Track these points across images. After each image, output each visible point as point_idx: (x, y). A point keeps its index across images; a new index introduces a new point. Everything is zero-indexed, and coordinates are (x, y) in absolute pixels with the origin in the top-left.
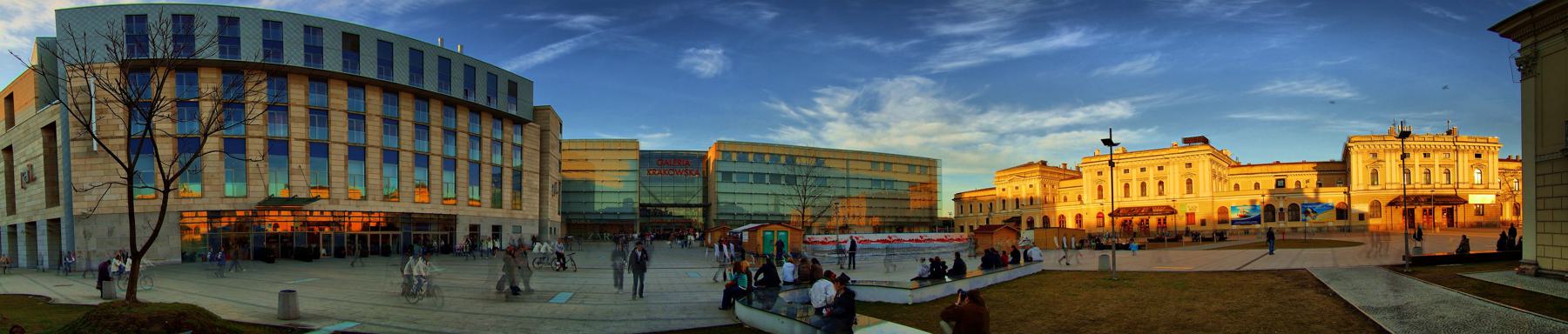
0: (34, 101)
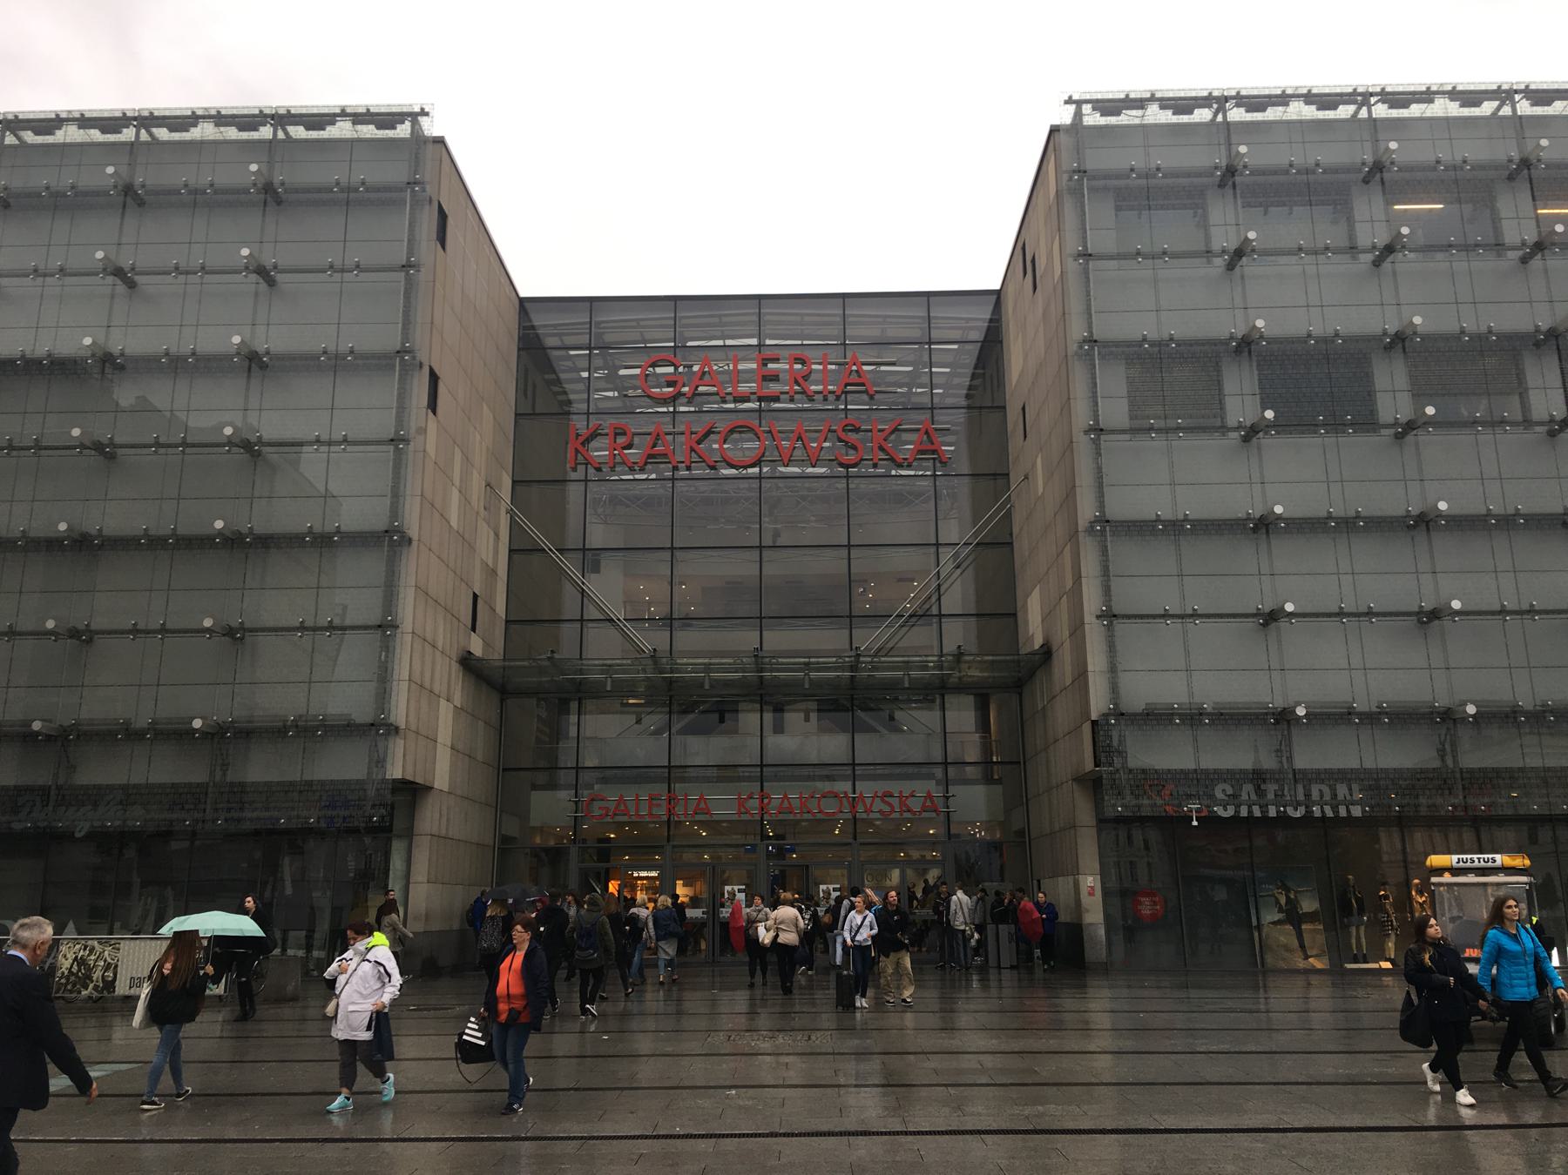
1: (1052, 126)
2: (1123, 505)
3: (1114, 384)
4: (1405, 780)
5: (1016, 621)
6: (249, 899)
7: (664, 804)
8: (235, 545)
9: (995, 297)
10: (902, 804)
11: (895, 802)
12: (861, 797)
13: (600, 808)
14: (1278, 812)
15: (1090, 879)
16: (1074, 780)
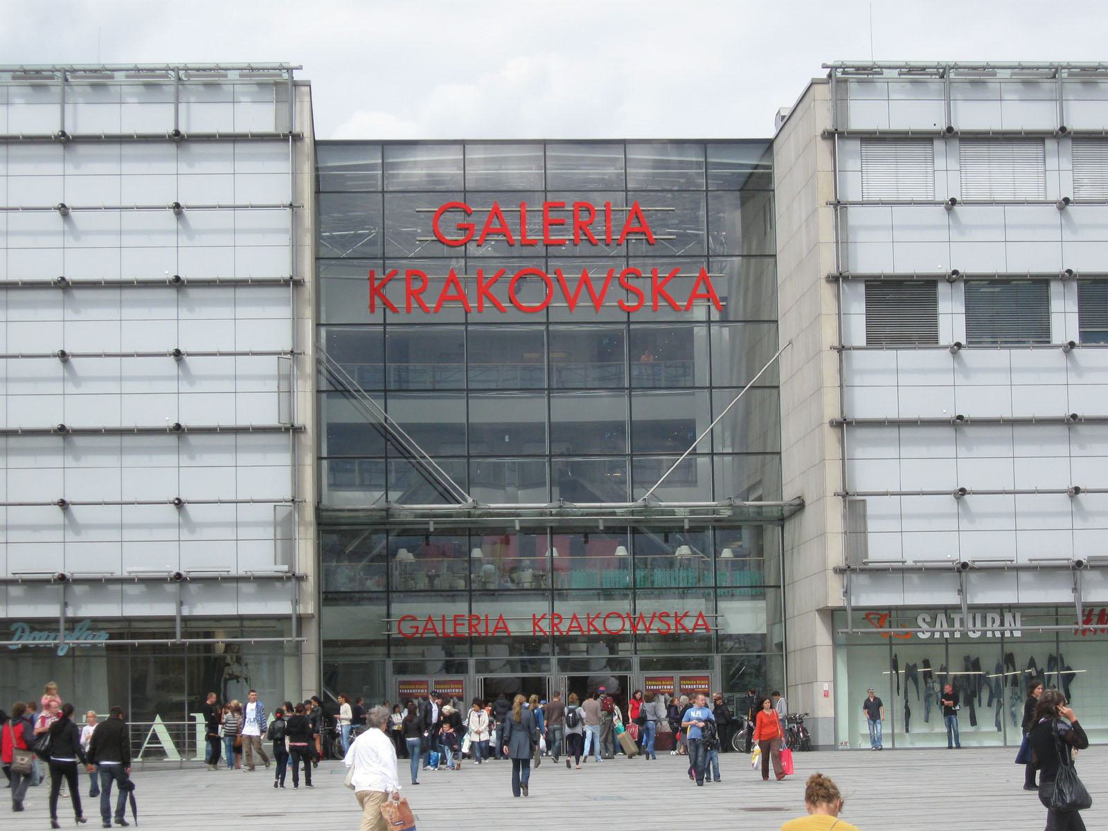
0: (783, 378)
1: (813, 79)
2: (866, 406)
3: (857, 309)
4: (547, 726)
5: (780, 458)
6: (208, 702)
7: (466, 623)
8: (556, 597)
9: (768, 145)
10: (678, 622)
11: (672, 622)
12: (641, 617)
13: (411, 627)
14: (413, 746)
15: (826, 684)
16: (818, 610)
